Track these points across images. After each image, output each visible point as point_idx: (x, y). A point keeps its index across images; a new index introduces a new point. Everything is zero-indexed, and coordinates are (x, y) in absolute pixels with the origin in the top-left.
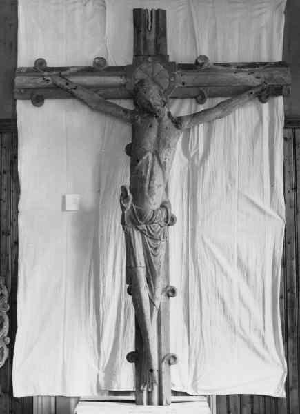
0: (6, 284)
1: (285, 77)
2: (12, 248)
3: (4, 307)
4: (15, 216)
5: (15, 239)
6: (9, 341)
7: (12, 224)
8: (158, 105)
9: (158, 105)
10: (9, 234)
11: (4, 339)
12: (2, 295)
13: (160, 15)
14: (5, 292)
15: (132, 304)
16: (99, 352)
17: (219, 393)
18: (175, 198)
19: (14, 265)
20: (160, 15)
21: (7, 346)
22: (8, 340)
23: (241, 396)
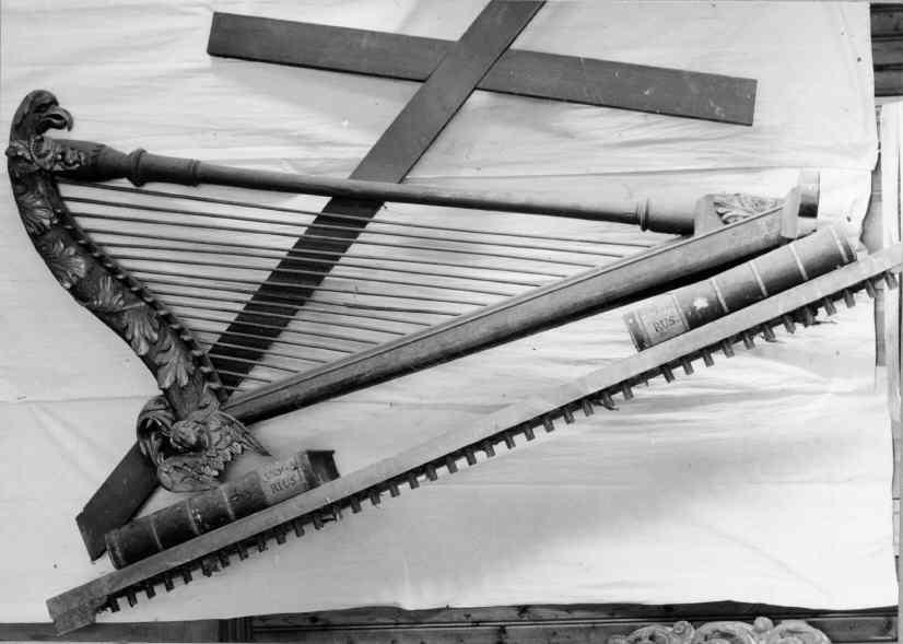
0: (629, 631)
1: (626, 390)
2: (537, 620)
3: (682, 634)
4: (455, 617)
5: (515, 614)
6: (766, 619)
7: (477, 623)
8: (39, 207)
9: (39, 207)
10: (502, 630)
11: (759, 632)
12: (652, 638)
13: (220, 20)
14: (645, 630)
15: (704, 327)
16: (783, 393)
17: (871, 90)
18: (564, 344)
19: (577, 614)
20: (220, 20)
21: (775, 625)
22: (762, 622)
23: (875, 37)
